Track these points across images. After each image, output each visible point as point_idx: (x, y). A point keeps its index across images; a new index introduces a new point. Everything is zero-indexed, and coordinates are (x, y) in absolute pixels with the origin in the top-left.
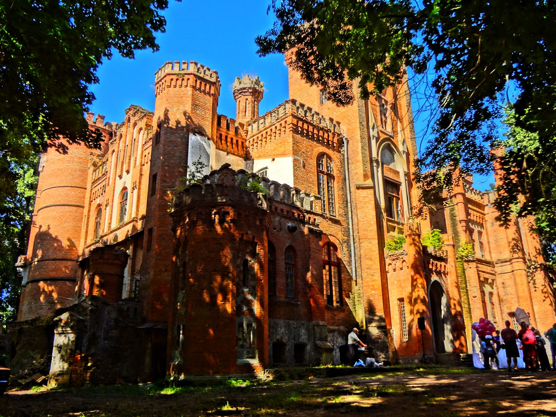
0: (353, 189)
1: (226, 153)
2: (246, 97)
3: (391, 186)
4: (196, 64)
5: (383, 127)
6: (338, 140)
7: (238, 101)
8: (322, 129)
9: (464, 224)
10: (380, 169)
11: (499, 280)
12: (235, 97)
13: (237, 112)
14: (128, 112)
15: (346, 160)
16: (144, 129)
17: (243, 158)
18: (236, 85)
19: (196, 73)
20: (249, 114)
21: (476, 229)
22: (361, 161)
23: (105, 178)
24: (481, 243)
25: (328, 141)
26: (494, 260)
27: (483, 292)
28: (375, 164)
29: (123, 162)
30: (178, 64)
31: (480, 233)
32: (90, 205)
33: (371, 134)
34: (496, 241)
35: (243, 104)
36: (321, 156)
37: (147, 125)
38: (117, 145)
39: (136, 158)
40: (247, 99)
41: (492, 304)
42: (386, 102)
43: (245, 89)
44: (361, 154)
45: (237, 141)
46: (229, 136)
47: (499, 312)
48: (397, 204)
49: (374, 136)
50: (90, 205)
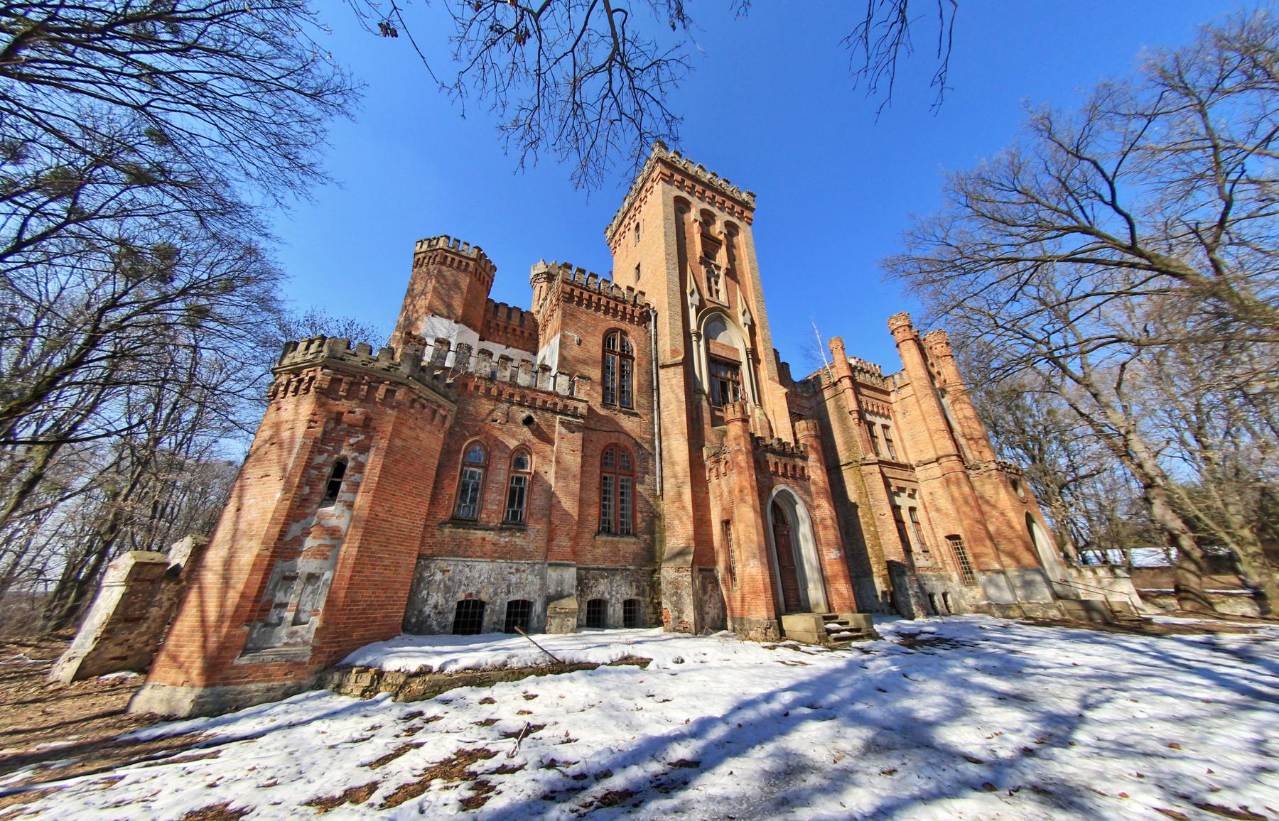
3: (723, 366)
4: (448, 238)
8: (615, 299)
9: (855, 415)
10: (702, 343)
11: (923, 489)
21: (879, 421)
24: (889, 441)
26: (913, 463)
27: (896, 509)
31: (885, 427)
34: (913, 437)
41: (916, 523)
42: (718, 268)
48: (735, 394)
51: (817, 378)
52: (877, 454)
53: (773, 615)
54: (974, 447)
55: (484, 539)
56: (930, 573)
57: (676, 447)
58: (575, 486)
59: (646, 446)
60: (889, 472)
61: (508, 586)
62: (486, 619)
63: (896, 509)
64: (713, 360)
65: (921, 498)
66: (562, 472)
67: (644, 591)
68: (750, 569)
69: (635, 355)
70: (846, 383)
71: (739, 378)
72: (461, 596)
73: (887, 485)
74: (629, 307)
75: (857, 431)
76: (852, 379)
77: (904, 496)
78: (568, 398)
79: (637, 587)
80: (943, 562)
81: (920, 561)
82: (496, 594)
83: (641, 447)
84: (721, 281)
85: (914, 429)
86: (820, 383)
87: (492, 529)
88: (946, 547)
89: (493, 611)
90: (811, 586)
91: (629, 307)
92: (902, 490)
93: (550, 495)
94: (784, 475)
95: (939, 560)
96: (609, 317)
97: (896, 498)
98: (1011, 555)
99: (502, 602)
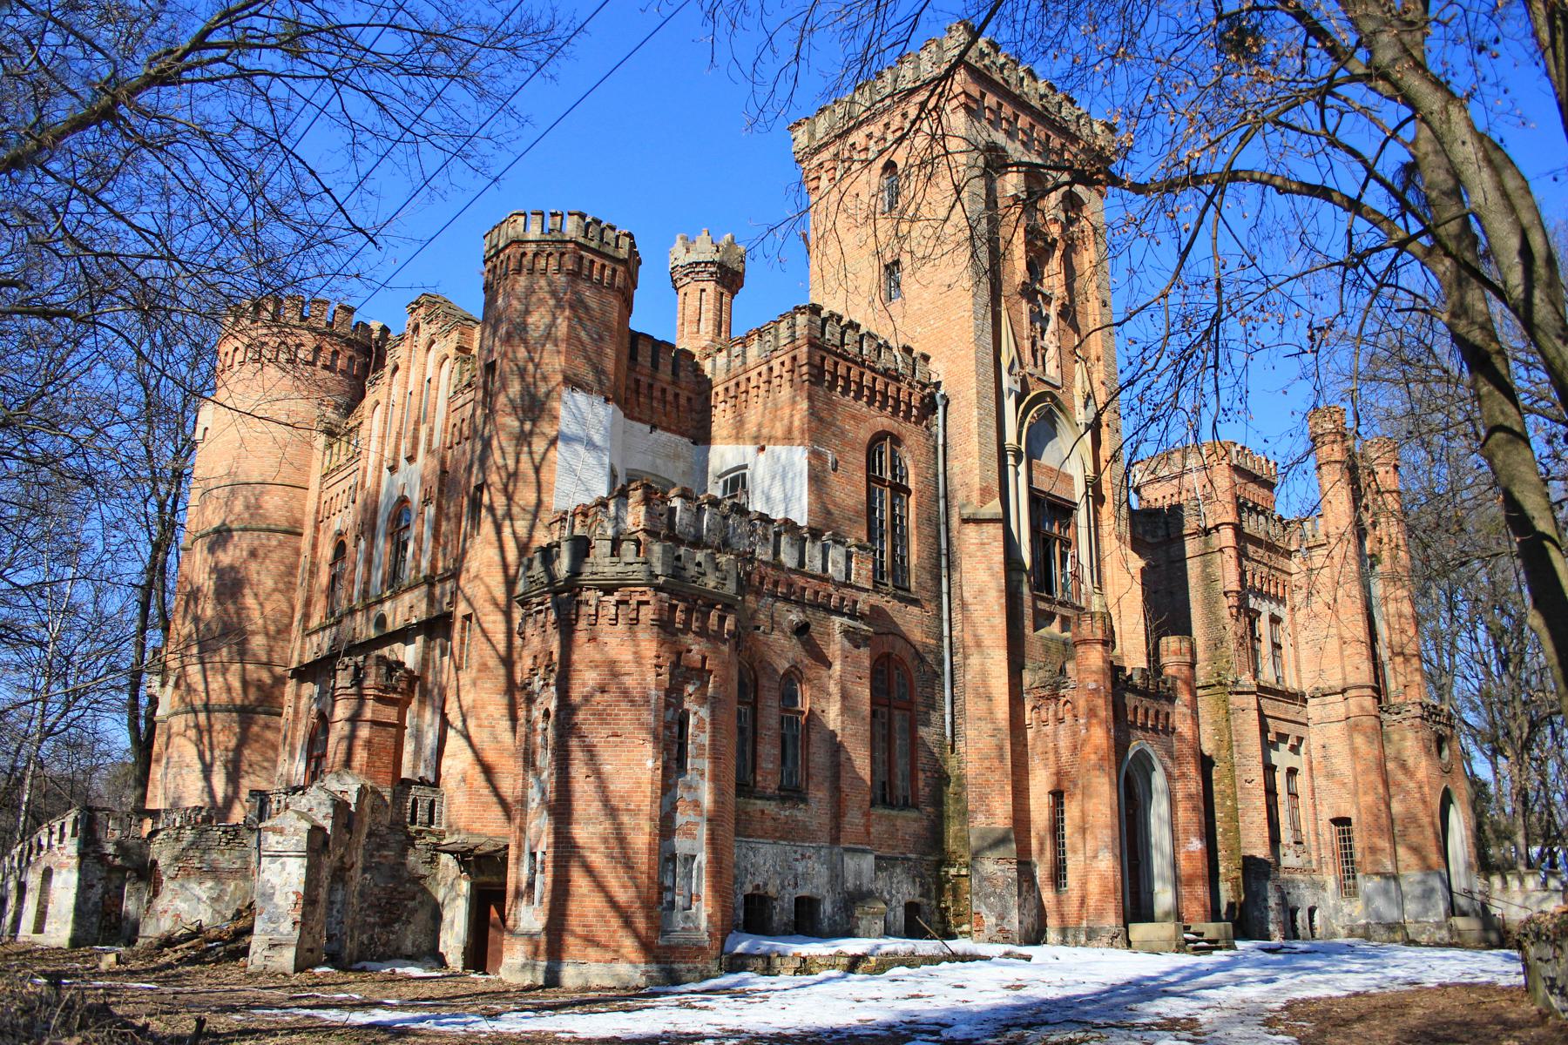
0: (955, 521)
1: (648, 428)
2: (702, 285)
3: (1050, 511)
4: (582, 216)
5: (1036, 365)
6: (922, 399)
7: (682, 291)
10: (1022, 468)
11: (1314, 738)
12: (674, 282)
13: (679, 322)
14: (414, 310)
15: (940, 449)
16: (452, 357)
17: (689, 437)
18: (680, 255)
19: (581, 240)
20: (707, 327)
21: (1266, 608)
22: (976, 455)
23: (354, 467)
25: (897, 401)
26: (1307, 688)
27: (1269, 769)
28: (1011, 460)
29: (399, 434)
30: (539, 218)
31: (1275, 620)
32: (317, 528)
33: (1005, 386)
35: (692, 302)
36: (879, 437)
37: (460, 349)
38: (386, 388)
39: (432, 429)
40: (703, 290)
41: (1293, 795)
42: (1048, 299)
43: (698, 264)
44: (976, 438)
45: (677, 396)
46: (658, 385)
47: (1311, 817)
48: (1064, 557)
49: (1010, 391)
50: (317, 528)
51: (1176, 510)
52: (1256, 673)
53: (1121, 922)
54: (1400, 669)
55: (763, 812)
56: (1299, 877)
57: (988, 665)
58: (864, 729)
59: (930, 658)
60: (1270, 707)
61: (796, 877)
62: (776, 918)
63: (1269, 769)
64: (1036, 498)
65: (1308, 752)
66: (848, 707)
67: (929, 890)
68: (1094, 864)
69: (912, 486)
70: (1227, 537)
71: (1070, 534)
72: (749, 889)
73: (1264, 729)
74: (904, 386)
75: (1233, 630)
76: (1238, 529)
77: (1284, 748)
78: (845, 585)
79: (922, 885)
80: (1320, 862)
81: (1289, 859)
82: (783, 887)
83: (922, 660)
84: (1051, 326)
85: (1317, 643)
86: (1181, 525)
87: (769, 799)
88: (1329, 834)
89: (782, 909)
90: (1158, 886)
91: (904, 386)
92: (1283, 738)
93: (836, 748)
94: (1144, 727)
95: (1314, 856)
96: (874, 410)
97: (1273, 754)
98: (1416, 850)
99: (789, 896)
